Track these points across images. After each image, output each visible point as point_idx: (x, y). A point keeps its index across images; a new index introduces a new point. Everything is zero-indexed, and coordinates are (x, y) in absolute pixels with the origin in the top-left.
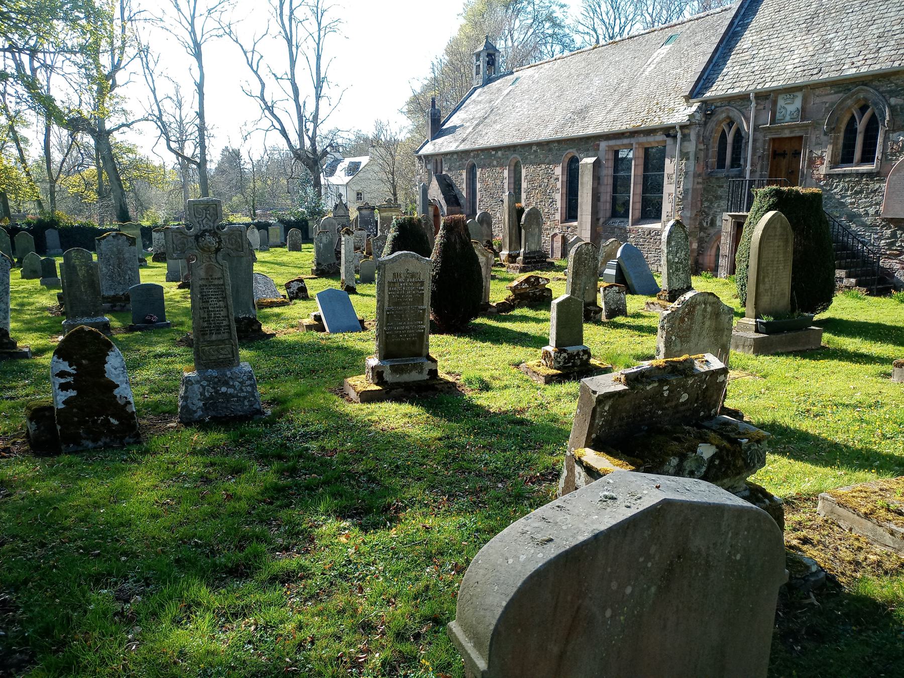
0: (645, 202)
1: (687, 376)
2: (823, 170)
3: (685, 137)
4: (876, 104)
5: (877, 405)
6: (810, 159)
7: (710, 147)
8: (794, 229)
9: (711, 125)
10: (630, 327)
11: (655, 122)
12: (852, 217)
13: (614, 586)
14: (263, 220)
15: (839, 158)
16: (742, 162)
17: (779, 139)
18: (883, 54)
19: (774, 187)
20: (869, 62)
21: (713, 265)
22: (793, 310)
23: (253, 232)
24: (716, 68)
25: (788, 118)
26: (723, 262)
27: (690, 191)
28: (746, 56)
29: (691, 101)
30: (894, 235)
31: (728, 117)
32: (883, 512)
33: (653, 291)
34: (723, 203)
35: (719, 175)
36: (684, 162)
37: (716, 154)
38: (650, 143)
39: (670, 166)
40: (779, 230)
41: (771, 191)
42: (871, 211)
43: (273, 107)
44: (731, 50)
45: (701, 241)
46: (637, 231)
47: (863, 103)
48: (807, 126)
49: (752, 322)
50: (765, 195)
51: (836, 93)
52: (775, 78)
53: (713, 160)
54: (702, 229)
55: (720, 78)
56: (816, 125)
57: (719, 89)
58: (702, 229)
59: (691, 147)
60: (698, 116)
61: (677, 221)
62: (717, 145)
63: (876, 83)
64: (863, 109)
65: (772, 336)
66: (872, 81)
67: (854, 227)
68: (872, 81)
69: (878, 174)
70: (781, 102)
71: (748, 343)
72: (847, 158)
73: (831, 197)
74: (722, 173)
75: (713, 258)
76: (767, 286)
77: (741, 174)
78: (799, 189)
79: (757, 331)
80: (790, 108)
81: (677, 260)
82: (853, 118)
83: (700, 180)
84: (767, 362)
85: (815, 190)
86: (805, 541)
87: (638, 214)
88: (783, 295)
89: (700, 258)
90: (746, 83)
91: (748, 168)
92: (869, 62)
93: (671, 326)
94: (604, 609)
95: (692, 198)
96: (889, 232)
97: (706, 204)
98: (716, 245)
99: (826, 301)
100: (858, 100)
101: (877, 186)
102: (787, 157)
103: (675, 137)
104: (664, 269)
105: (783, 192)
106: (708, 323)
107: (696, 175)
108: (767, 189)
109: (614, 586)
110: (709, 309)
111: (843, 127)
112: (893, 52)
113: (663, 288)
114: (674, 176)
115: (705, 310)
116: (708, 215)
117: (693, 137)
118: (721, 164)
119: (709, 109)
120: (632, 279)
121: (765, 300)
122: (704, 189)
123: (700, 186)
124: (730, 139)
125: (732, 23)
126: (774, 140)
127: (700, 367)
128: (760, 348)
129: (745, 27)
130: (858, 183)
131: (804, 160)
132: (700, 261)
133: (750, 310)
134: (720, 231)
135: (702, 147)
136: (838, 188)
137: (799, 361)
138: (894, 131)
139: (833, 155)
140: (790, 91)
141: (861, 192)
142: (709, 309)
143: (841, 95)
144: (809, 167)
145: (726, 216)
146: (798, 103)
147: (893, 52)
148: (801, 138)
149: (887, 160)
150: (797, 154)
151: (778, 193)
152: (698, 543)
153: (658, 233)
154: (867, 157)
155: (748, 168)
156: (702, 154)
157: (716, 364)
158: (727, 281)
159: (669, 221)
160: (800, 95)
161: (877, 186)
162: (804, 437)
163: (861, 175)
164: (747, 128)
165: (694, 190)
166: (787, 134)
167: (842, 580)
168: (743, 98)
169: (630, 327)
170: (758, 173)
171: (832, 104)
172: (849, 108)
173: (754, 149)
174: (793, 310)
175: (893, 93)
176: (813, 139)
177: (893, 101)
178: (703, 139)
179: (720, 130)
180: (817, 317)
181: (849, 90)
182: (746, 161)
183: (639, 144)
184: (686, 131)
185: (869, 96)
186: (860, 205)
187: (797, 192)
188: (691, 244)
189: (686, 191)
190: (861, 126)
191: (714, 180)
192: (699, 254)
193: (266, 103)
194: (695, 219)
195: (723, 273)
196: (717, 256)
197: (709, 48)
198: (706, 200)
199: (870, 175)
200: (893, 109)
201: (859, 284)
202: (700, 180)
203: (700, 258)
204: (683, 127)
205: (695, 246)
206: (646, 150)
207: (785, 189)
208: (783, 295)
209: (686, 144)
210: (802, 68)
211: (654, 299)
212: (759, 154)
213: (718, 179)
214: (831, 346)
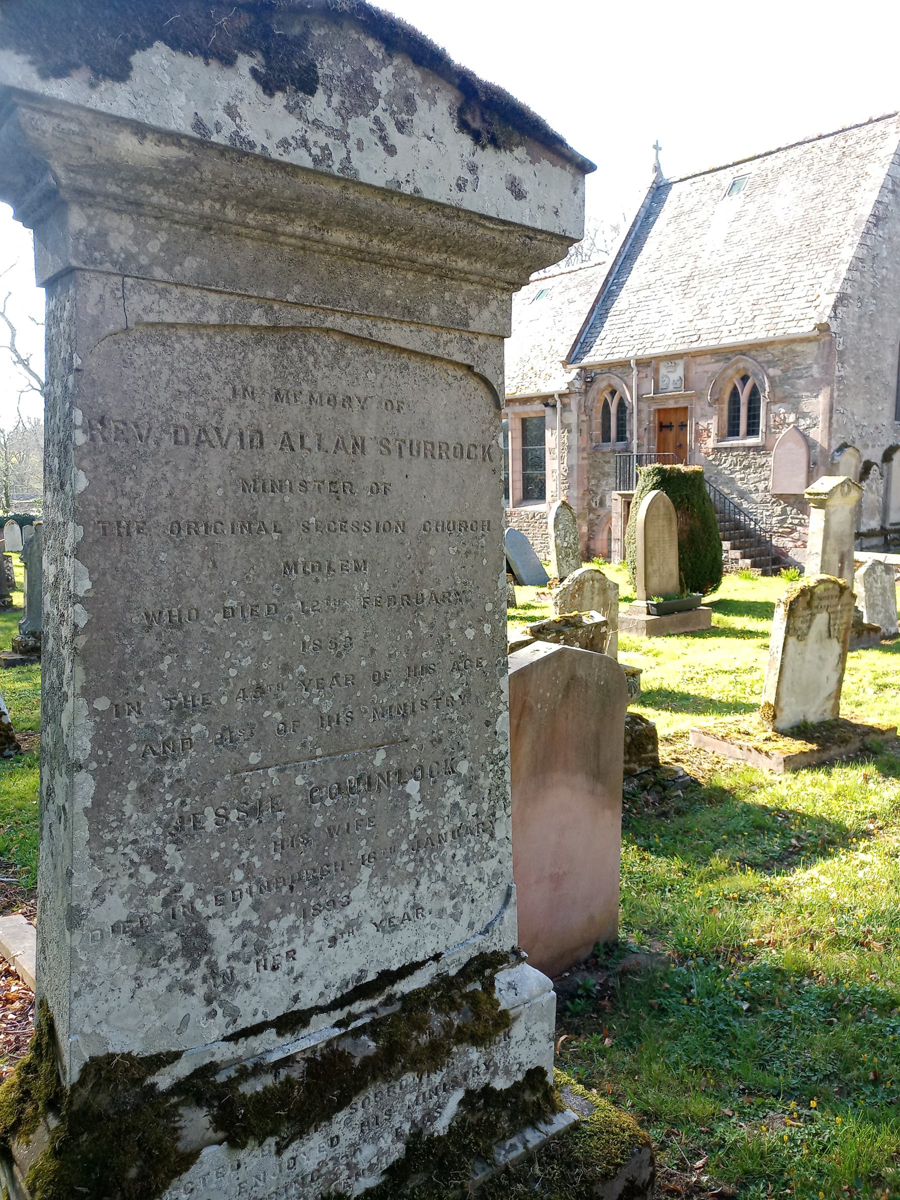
0: (527, 480)
1: (577, 627)
2: (711, 443)
3: (565, 407)
4: (755, 375)
5: (751, 670)
6: (697, 431)
7: (593, 418)
8: (677, 508)
9: (592, 394)
10: (521, 619)
11: (530, 391)
12: (743, 495)
13: (541, 691)
14: (21, 512)
15: (725, 431)
16: (628, 435)
17: (665, 410)
18: (759, 321)
19: (657, 465)
20: (745, 330)
21: (605, 551)
22: (682, 591)
23: (12, 529)
24: (593, 331)
25: (671, 388)
26: (616, 547)
27: (575, 468)
28: (626, 317)
29: (569, 366)
30: (784, 511)
31: (610, 385)
32: (735, 735)
33: (542, 580)
34: (612, 481)
35: (605, 450)
36: (566, 434)
37: (600, 426)
38: (527, 413)
39: (552, 439)
40: (662, 510)
41: (654, 469)
42: (761, 486)
43: (27, 360)
44: (607, 311)
45: (591, 525)
46: (520, 514)
47: (743, 373)
48: (690, 396)
49: (643, 604)
50: (649, 475)
51: (717, 361)
52: (655, 344)
53: (597, 433)
54: (591, 510)
55: (598, 341)
56: (700, 395)
57: (596, 356)
58: (591, 510)
59: (572, 418)
60: (578, 384)
61: (564, 502)
62: (600, 415)
63: (753, 353)
64: (745, 379)
65: (664, 618)
66: (749, 350)
67: (745, 505)
68: (749, 350)
69: (763, 448)
70: (663, 371)
71: (640, 626)
72: (733, 431)
73: (719, 473)
74: (608, 447)
75: (605, 543)
76: (655, 567)
77: (627, 449)
78: (680, 466)
79: (649, 613)
80: (672, 376)
81: (565, 544)
82: (735, 388)
83: (585, 455)
84: (659, 643)
85: (697, 468)
86: (677, 760)
87: (519, 494)
88: (671, 575)
89: (592, 543)
90: (625, 349)
91: (635, 442)
92: (745, 330)
93: (564, 603)
94: (537, 703)
95: (578, 476)
96: (779, 508)
97: (593, 482)
98: (607, 529)
99: (713, 579)
100: (738, 371)
101: (764, 460)
102: (674, 429)
103: (554, 406)
104: (553, 557)
105: (665, 471)
106: (596, 599)
107: (581, 450)
108: (650, 467)
109: (541, 691)
110: (597, 585)
111: (726, 397)
112: (769, 321)
113: (552, 577)
114: (557, 451)
115: (593, 586)
116: (596, 494)
117: (574, 406)
118: (606, 438)
119: (588, 377)
120: (519, 570)
121: (655, 582)
122: (590, 465)
123: (585, 462)
124: (613, 409)
125: (606, 281)
126: (659, 410)
127: (586, 621)
128: (653, 630)
129: (620, 285)
130: (746, 457)
131: (691, 433)
132: (592, 547)
133: (642, 593)
134: (610, 512)
135: (584, 418)
136: (728, 461)
137: (689, 639)
138: (775, 403)
139: (719, 428)
140: (672, 358)
141: (749, 467)
142: (597, 585)
143: (721, 364)
144: (696, 440)
145: (615, 494)
146: (680, 372)
147: (769, 321)
148: (686, 408)
149: (771, 433)
150: (683, 426)
151: (660, 471)
152: (581, 673)
153: (543, 516)
154: (752, 430)
155: (635, 442)
156: (585, 427)
157: (598, 618)
158: (620, 567)
159: (554, 501)
160: (681, 364)
161: (764, 460)
162: (686, 697)
163: (749, 448)
164: (631, 398)
165: (579, 466)
166: (671, 404)
167: (701, 781)
168: (624, 365)
169: (521, 619)
170: (645, 448)
171: (714, 373)
172: (731, 378)
173: (639, 421)
174: (682, 591)
175: (771, 363)
176: (699, 410)
177: (771, 372)
178: (585, 410)
179: (603, 399)
180: (707, 599)
181: (729, 359)
182: (631, 434)
183: (515, 414)
184: (566, 400)
185: (748, 366)
186: (745, 480)
187: (679, 470)
188: (580, 527)
189: (570, 468)
190: (744, 398)
191: (600, 455)
192: (590, 539)
193: (18, 356)
194: (583, 499)
195: (616, 558)
196: (609, 540)
197: (584, 305)
198: (593, 478)
199: (756, 449)
200: (771, 380)
201: (754, 565)
202: (585, 455)
203: (592, 542)
204: (561, 396)
205: (585, 529)
206: (524, 421)
207: (668, 467)
208: (671, 575)
209: (566, 414)
210: (682, 335)
211: (545, 590)
212: (644, 426)
213: (604, 453)
214: (721, 626)
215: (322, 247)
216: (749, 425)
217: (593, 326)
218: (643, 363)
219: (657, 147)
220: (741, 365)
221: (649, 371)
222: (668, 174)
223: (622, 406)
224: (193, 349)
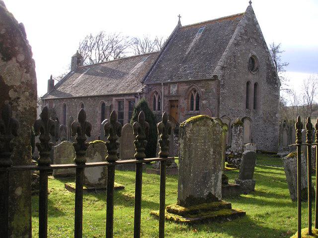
103: (138, 97)
219: (180, 17)
220: (194, 87)
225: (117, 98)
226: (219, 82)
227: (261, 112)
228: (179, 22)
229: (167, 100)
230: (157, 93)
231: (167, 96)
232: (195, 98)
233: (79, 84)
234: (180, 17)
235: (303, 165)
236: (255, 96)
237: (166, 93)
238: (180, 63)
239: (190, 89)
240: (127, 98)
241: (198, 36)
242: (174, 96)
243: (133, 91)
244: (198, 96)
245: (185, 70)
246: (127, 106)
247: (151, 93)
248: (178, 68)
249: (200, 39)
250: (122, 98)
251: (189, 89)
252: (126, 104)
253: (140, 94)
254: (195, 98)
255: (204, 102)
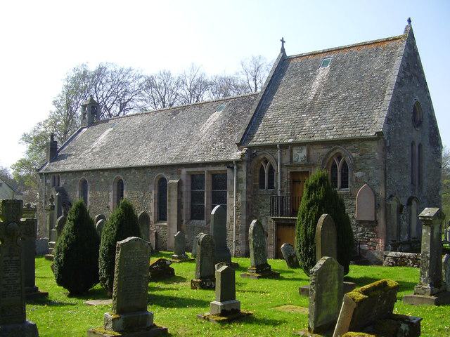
3: (238, 169)
30: (363, 231)
31: (264, 158)
59: (243, 174)
70: (295, 152)
72: (262, 186)
103: (233, 168)
140: (300, 145)
146: (304, 153)
215: (96, 77)
216: (342, 182)
217: (260, 112)
218: (284, 146)
219: (283, 41)
220: (338, 151)
221: (288, 151)
222: (289, 54)
223: (271, 170)
224: (414, 234)
225: (190, 170)
226: (385, 142)
227: (425, 189)
228: (283, 50)
229: (287, 172)
230: (266, 162)
231: (287, 166)
232: (266, 171)
233: (103, 149)
234: (283, 41)
235: (289, 274)
236: (419, 164)
237: (286, 159)
238: (304, 113)
239: (332, 154)
240: (211, 169)
241: (323, 72)
242: (300, 166)
243: (222, 158)
244: (345, 165)
245: (316, 125)
246: (210, 183)
247: (255, 161)
248: (302, 120)
249: (330, 76)
250: (200, 169)
251: (329, 153)
252: (207, 178)
253: (237, 162)
254: (266, 171)
255: (358, 174)
